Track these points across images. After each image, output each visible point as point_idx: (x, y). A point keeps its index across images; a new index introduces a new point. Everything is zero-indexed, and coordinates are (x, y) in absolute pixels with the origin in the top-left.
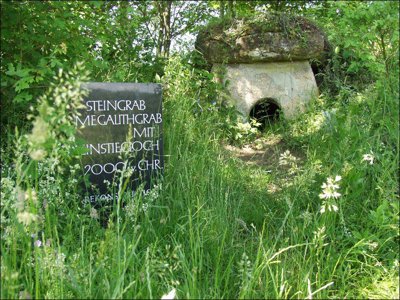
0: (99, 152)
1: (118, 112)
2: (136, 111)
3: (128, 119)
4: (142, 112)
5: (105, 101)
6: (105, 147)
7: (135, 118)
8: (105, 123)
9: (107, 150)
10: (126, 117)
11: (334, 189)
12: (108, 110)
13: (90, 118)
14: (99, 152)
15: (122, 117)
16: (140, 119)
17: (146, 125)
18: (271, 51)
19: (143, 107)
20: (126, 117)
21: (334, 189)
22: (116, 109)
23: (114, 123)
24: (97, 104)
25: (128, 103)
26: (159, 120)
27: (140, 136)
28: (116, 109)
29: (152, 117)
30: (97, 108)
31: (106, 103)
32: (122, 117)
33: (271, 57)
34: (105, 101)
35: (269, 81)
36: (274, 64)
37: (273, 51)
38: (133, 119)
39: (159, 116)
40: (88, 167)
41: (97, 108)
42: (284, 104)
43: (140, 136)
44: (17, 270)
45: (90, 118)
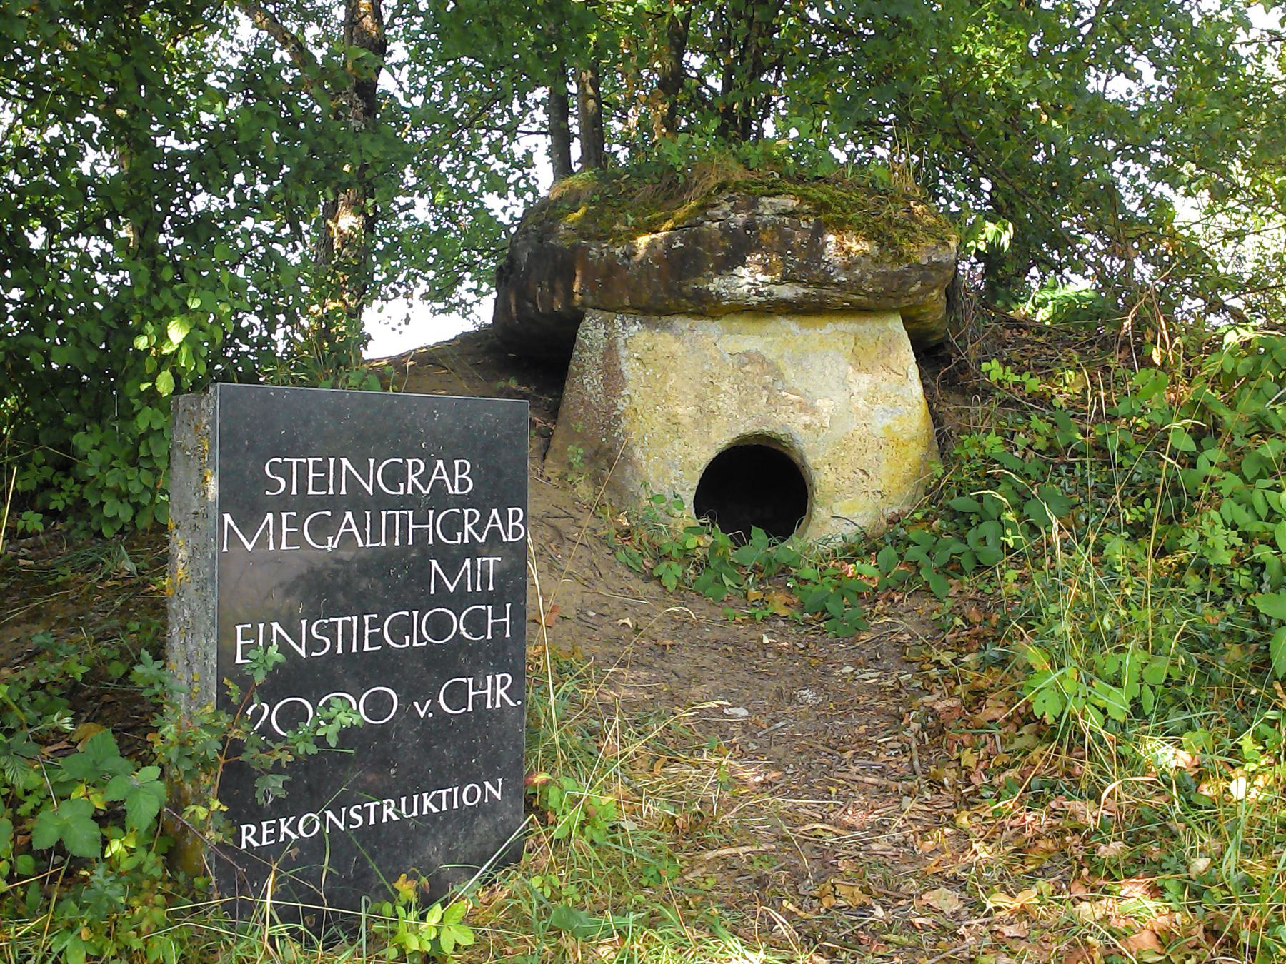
0: (302, 652)
1: (380, 502)
2: (439, 497)
3: (411, 526)
4: (462, 502)
5: (332, 460)
6: (330, 631)
7: (434, 527)
8: (332, 544)
9: (334, 643)
10: (404, 520)
11: (1181, 190)
12: (343, 492)
13: (278, 520)
14: (302, 652)
15: (390, 519)
16: (452, 526)
17: (472, 550)
18: (786, 279)
19: (463, 484)
20: (404, 520)
21: (1181, 190)
22: (370, 490)
23: (365, 543)
24: (303, 469)
25: (416, 467)
26: (516, 531)
27: (452, 589)
28: (370, 490)
29: (494, 522)
30: (302, 487)
31: (338, 466)
32: (390, 519)
33: (785, 301)
34: (332, 460)
35: (769, 379)
36: (780, 318)
37: (794, 280)
38: (430, 526)
39: (516, 515)
40: (258, 713)
41: (302, 487)
42: (825, 476)
43: (452, 589)
44: (351, 942)
45: (278, 520)
